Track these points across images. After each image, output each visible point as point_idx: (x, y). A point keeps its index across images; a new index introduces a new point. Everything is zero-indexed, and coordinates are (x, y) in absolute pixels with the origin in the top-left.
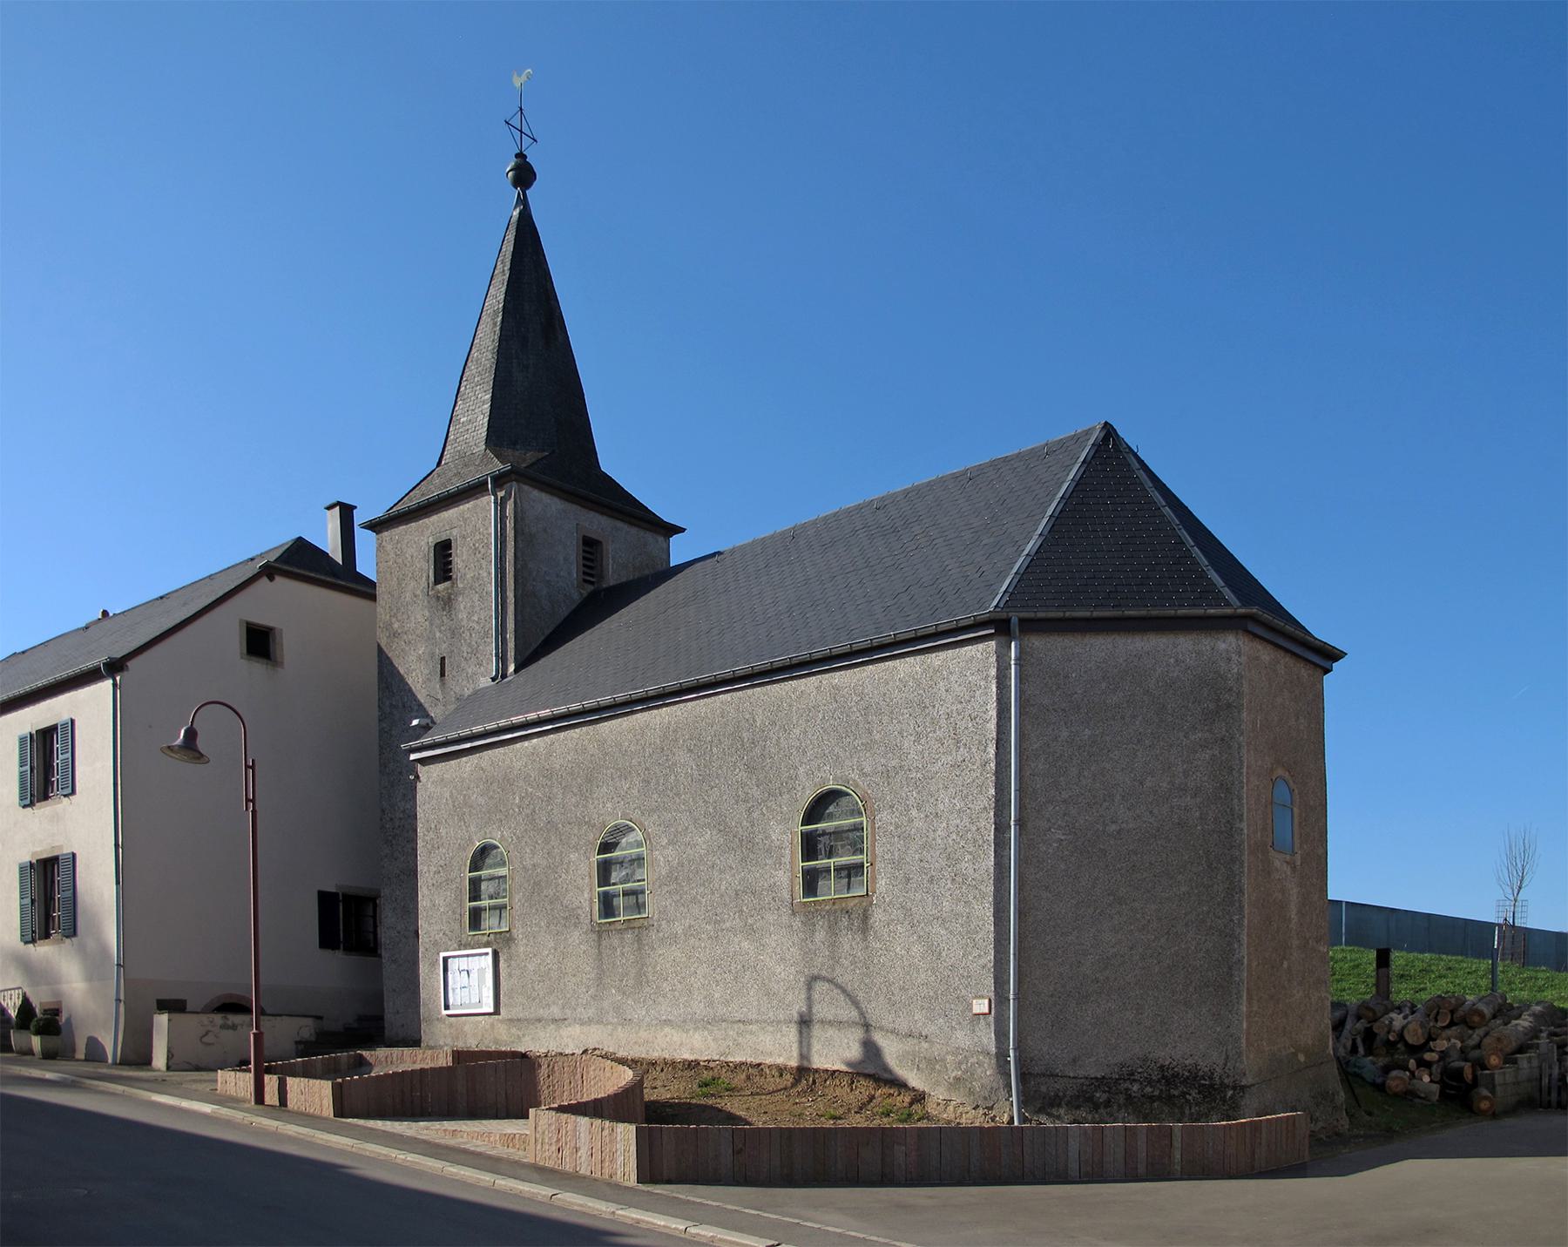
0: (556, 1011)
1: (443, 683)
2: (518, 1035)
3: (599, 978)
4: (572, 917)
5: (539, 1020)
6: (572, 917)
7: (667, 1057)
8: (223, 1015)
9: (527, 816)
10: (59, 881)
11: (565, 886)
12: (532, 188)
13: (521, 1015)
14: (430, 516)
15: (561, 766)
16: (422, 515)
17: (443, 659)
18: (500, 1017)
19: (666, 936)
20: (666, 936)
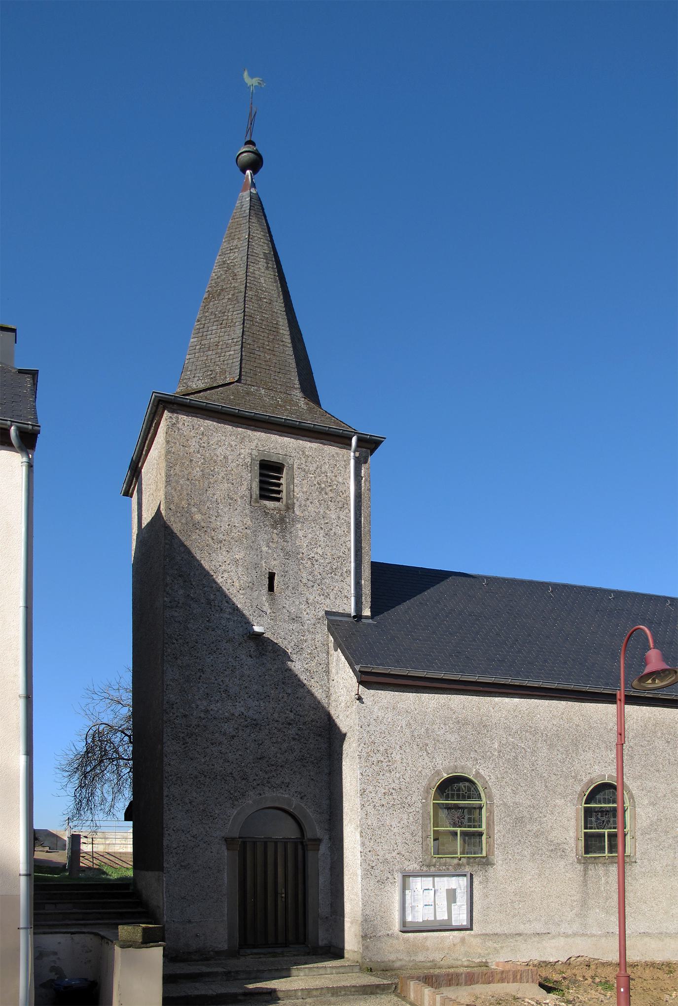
0: (539, 927)
1: (272, 600)
2: (495, 948)
3: (584, 903)
4: (557, 850)
5: (520, 935)
6: (557, 850)
7: (647, 960)
8: (420, 958)
9: (508, 760)
10: (582, 837)
11: (550, 824)
12: (258, 173)
13: (498, 931)
14: (255, 430)
15: (546, 727)
16: (210, 417)
17: (271, 576)
18: (472, 932)
19: (647, 871)
20: (647, 871)
